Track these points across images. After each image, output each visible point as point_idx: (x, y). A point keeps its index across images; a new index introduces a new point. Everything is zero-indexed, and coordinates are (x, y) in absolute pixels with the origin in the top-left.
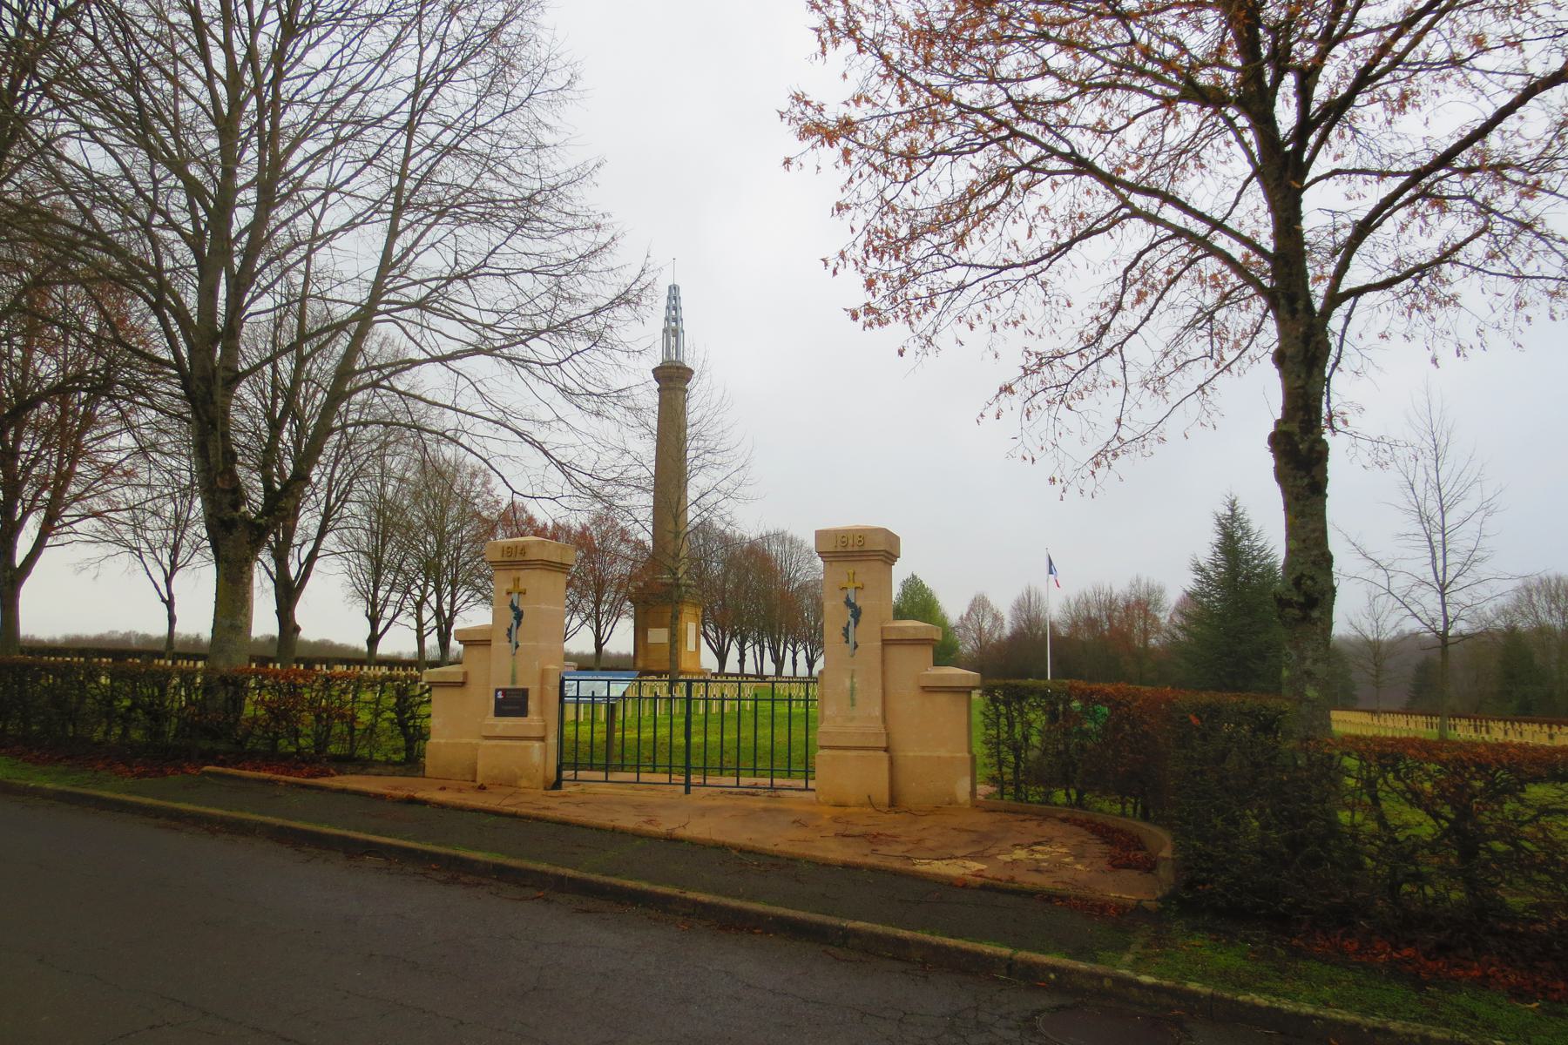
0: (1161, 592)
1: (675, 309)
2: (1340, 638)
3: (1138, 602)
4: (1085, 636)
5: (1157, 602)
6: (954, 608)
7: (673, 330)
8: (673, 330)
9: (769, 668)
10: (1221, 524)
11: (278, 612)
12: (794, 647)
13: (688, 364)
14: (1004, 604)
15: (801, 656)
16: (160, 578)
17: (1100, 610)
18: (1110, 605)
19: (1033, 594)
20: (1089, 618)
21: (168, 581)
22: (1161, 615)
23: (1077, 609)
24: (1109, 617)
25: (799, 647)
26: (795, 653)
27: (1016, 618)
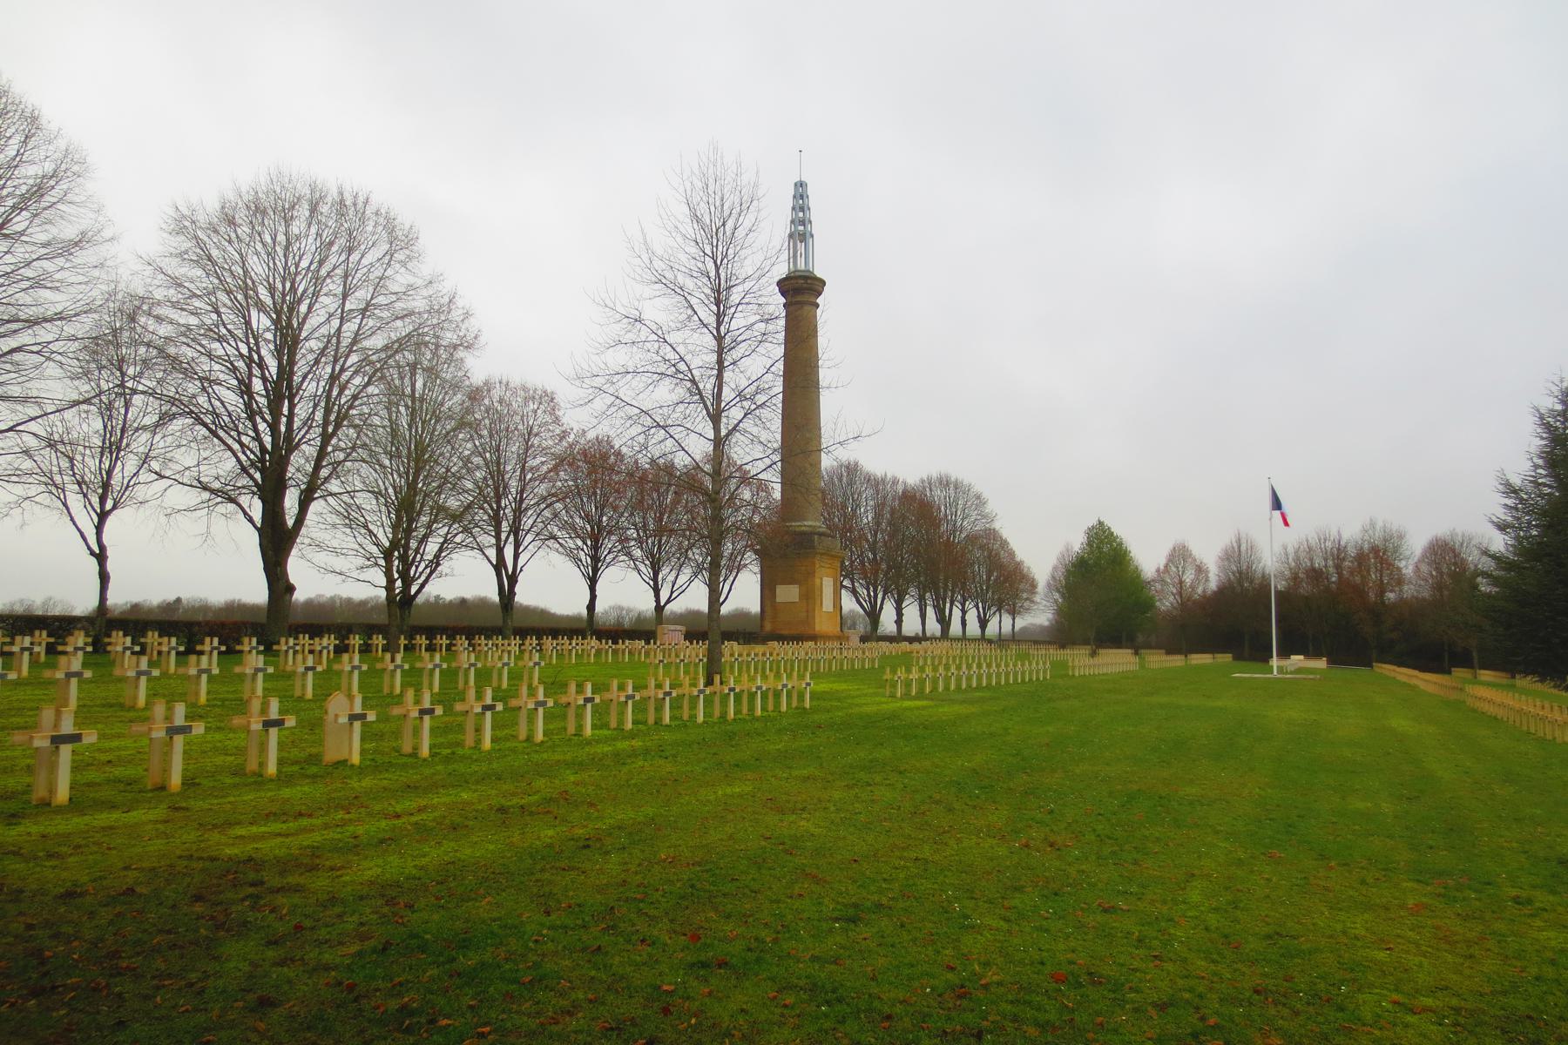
0: (1401, 537)
1: (802, 197)
2: (309, 604)
3: (1375, 550)
4: (1305, 589)
5: (1396, 549)
6: (1148, 558)
7: (800, 233)
8: (800, 233)
9: (933, 627)
10: (1547, 426)
11: (265, 569)
12: (963, 605)
13: (818, 273)
14: (1210, 555)
15: (972, 616)
16: (88, 526)
17: (1326, 560)
18: (1339, 554)
19: (1243, 541)
20: (1313, 569)
21: (99, 529)
22: (1402, 564)
23: (1297, 559)
24: (1338, 567)
25: (969, 605)
26: (964, 612)
27: (1223, 569)
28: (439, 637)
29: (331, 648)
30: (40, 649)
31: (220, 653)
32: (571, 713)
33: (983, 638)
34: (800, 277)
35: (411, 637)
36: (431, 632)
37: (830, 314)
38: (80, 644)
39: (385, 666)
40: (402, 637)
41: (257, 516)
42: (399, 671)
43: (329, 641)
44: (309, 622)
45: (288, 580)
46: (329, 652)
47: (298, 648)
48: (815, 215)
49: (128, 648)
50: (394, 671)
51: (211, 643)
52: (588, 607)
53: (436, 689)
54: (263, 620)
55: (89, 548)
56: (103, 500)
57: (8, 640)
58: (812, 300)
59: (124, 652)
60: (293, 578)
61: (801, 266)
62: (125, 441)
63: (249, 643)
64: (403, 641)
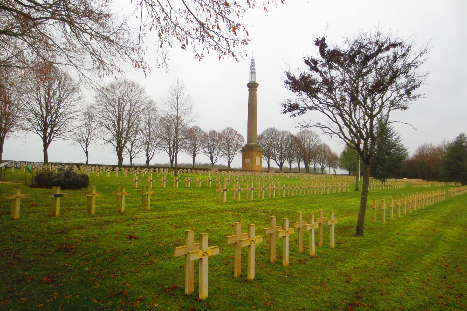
8: (253, 72)
13: (257, 83)
16: (84, 147)
30: (104, 169)
32: (248, 192)
33: (335, 174)
34: (252, 83)
37: (259, 92)
41: (116, 145)
48: (256, 67)
52: (122, 159)
56: (87, 143)
58: (255, 88)
61: (253, 80)
62: (53, 135)
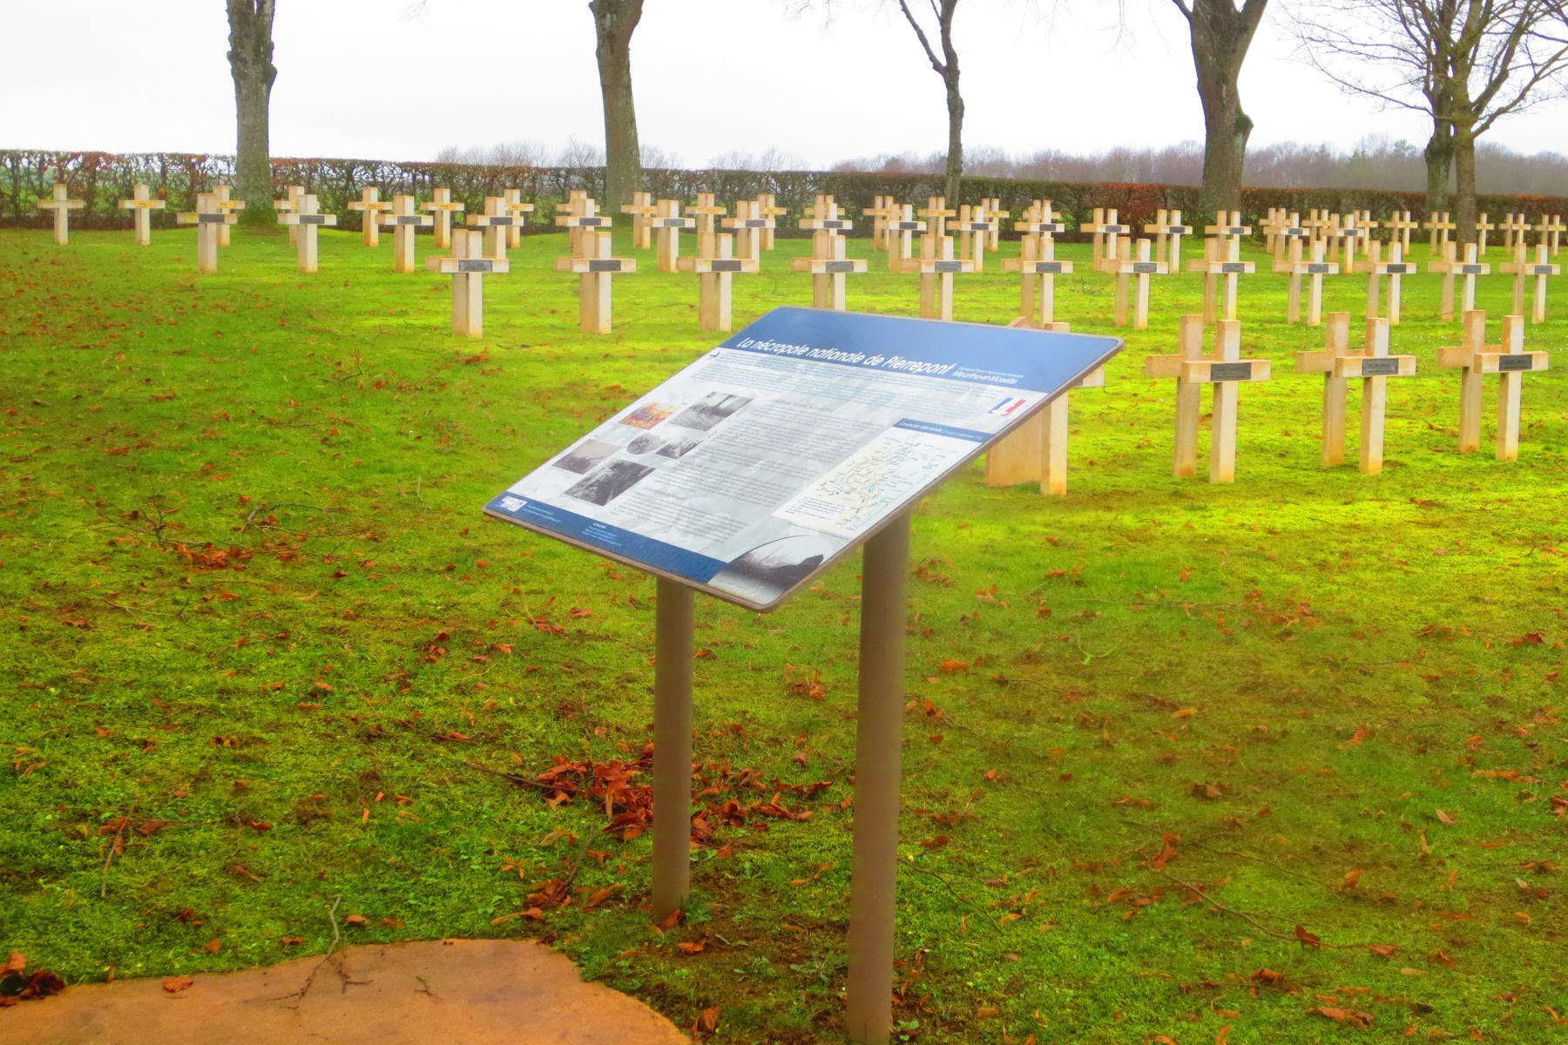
28: (1546, 218)
29: (771, 224)
31: (1243, 239)
35: (1496, 218)
36: (1498, 207)
38: (833, 217)
39: (1445, 269)
40: (1484, 217)
42: (1471, 278)
43: (989, 213)
44: (729, 166)
45: (1239, 110)
46: (764, 233)
47: (922, 226)
49: (673, 223)
50: (1460, 279)
51: (1168, 221)
52: (269, 75)
53: (1395, 314)
54: (1197, 183)
55: (932, 58)
57: (952, 213)
59: (901, 233)
60: (1248, 105)
63: (1103, 222)
64: (1484, 225)
